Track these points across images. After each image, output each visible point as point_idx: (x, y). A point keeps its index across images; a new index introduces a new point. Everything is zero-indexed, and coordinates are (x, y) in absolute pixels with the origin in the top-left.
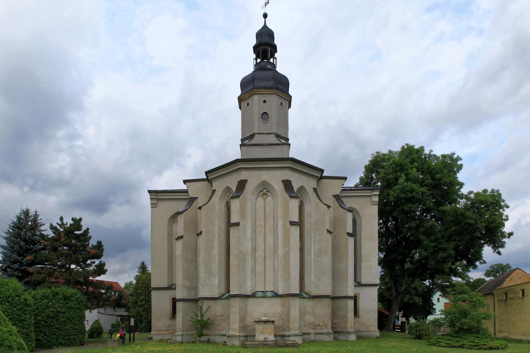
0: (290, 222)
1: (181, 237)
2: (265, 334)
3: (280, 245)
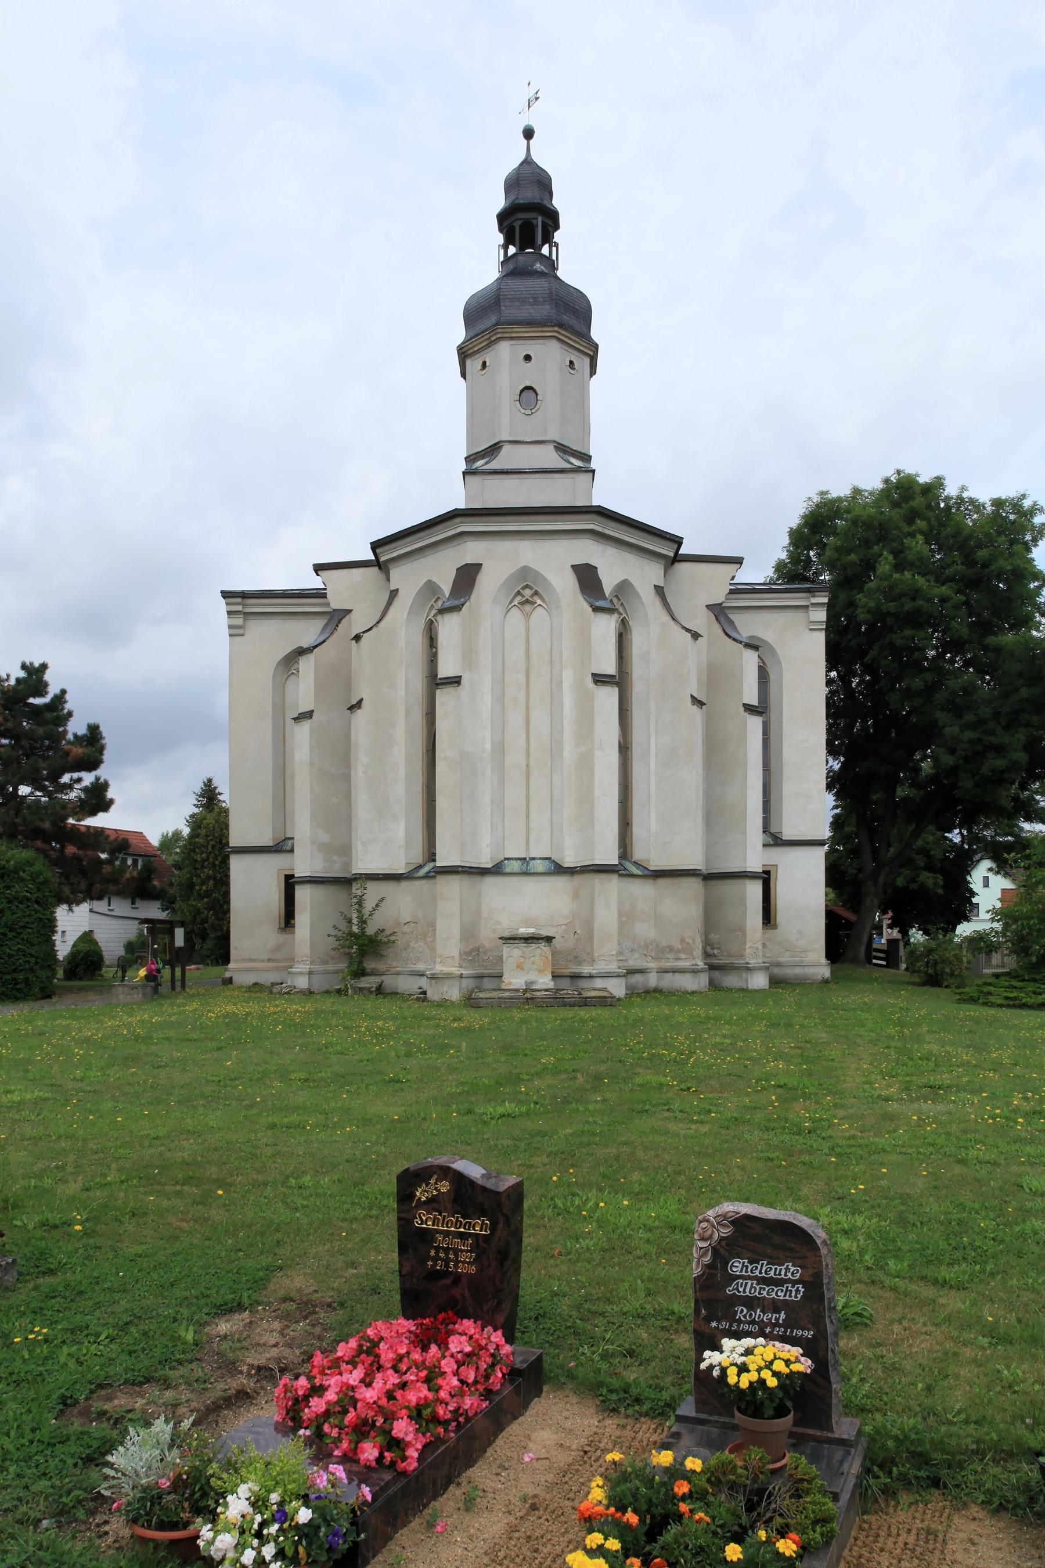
1: (309, 715)
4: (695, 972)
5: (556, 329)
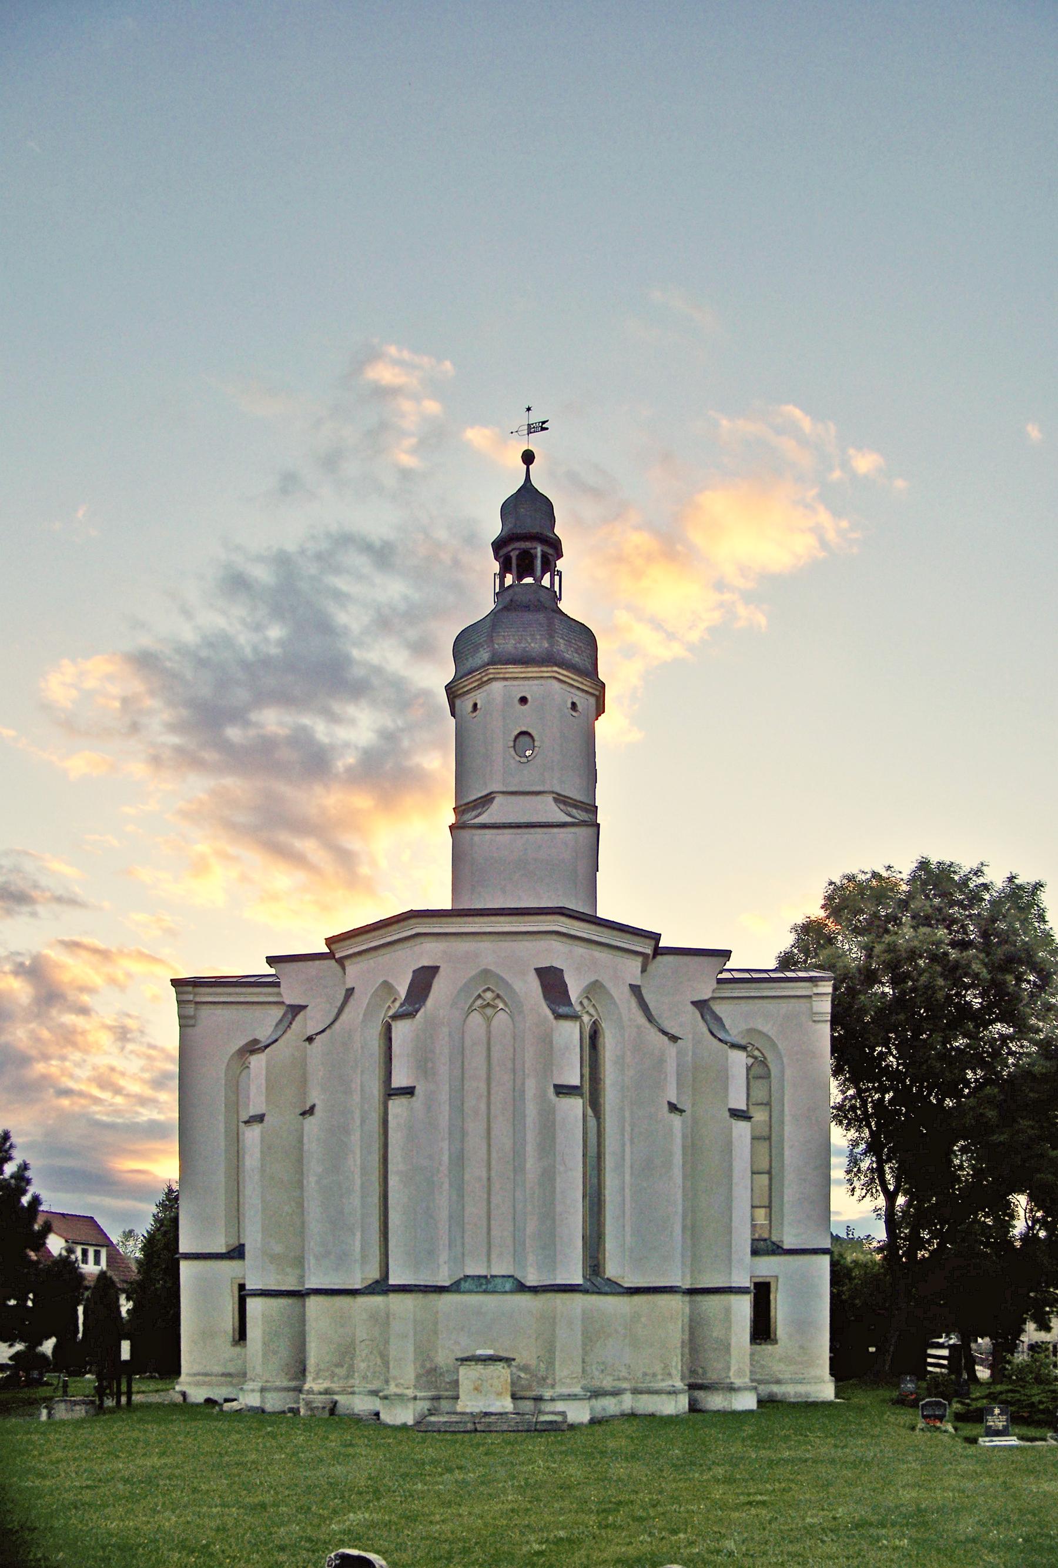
0: (556, 1086)
1: (260, 1118)
2: (484, 1395)
3: (531, 1149)
4: (673, 1392)
5: (556, 669)
